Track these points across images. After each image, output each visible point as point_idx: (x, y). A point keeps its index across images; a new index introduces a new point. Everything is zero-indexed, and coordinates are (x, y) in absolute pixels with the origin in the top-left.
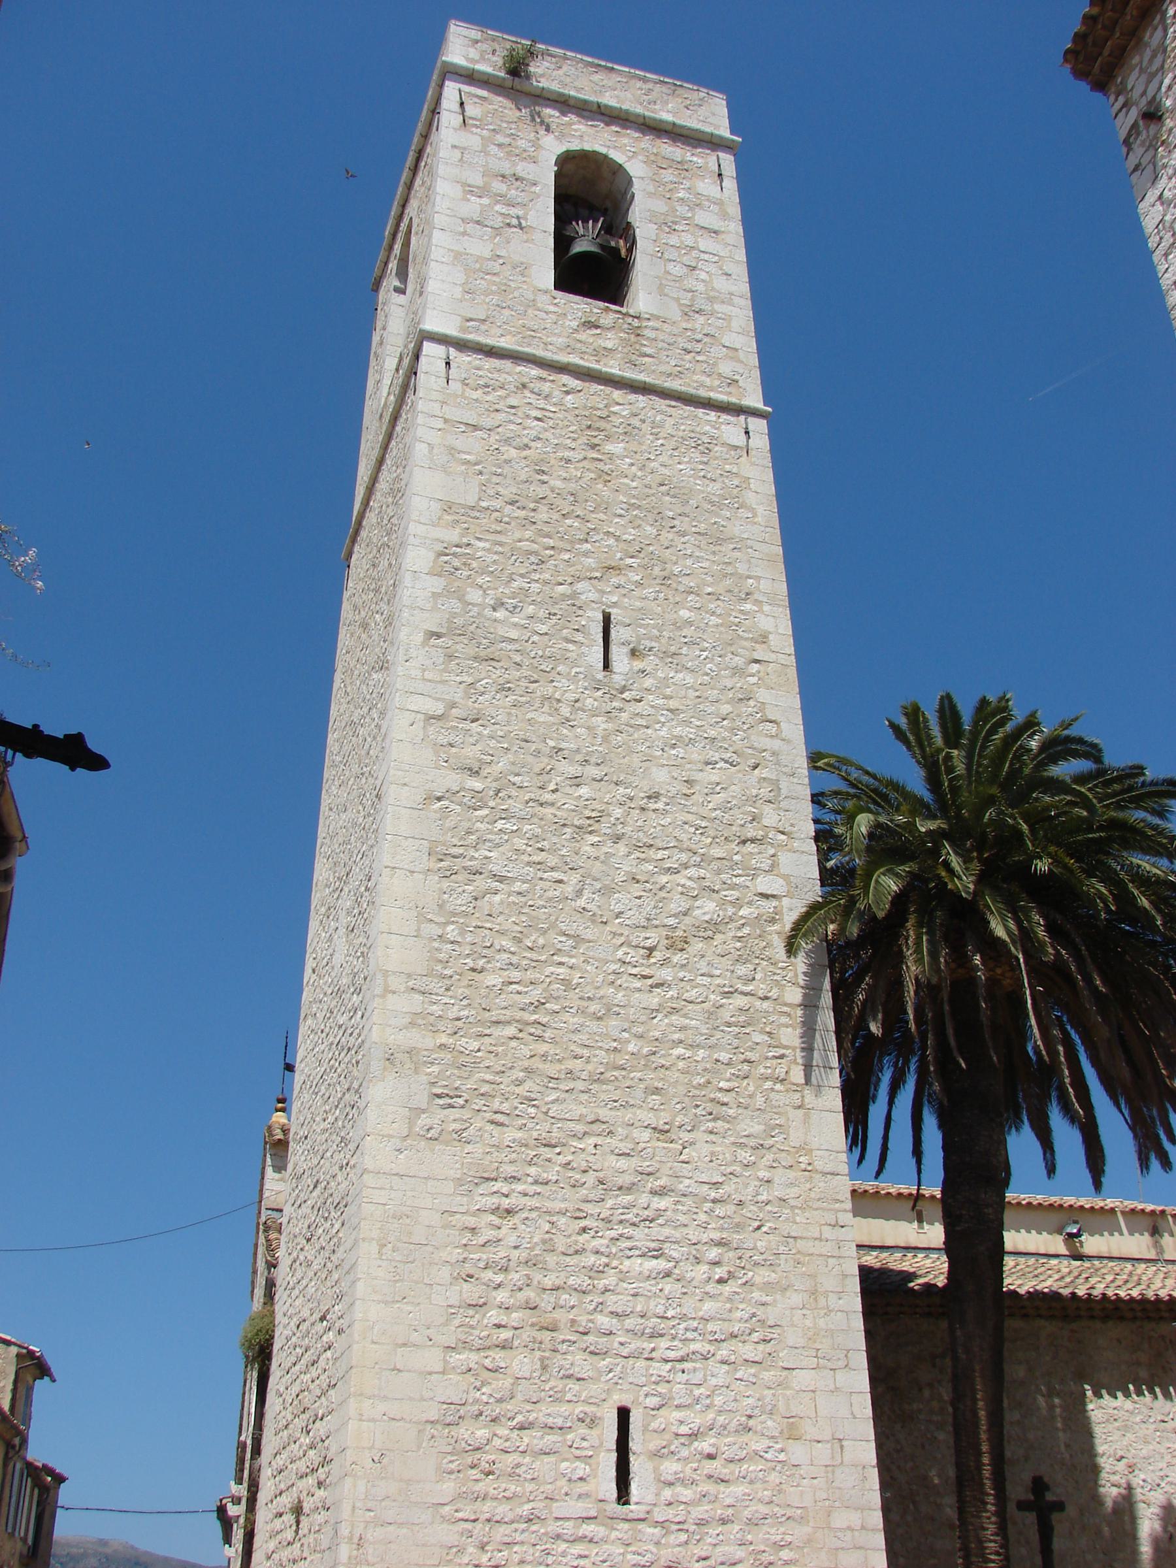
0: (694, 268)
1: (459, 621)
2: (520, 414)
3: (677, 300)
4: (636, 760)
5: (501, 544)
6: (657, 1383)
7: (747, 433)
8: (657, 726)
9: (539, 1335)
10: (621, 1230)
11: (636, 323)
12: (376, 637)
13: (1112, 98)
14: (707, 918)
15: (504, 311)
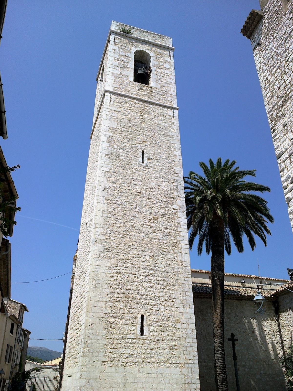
1: (112, 152)
2: (126, 108)
4: (148, 181)
5: (121, 136)
7: (174, 113)
8: (153, 174)
9: (125, 299)
12: (96, 155)
14: (162, 213)
15: (123, 86)
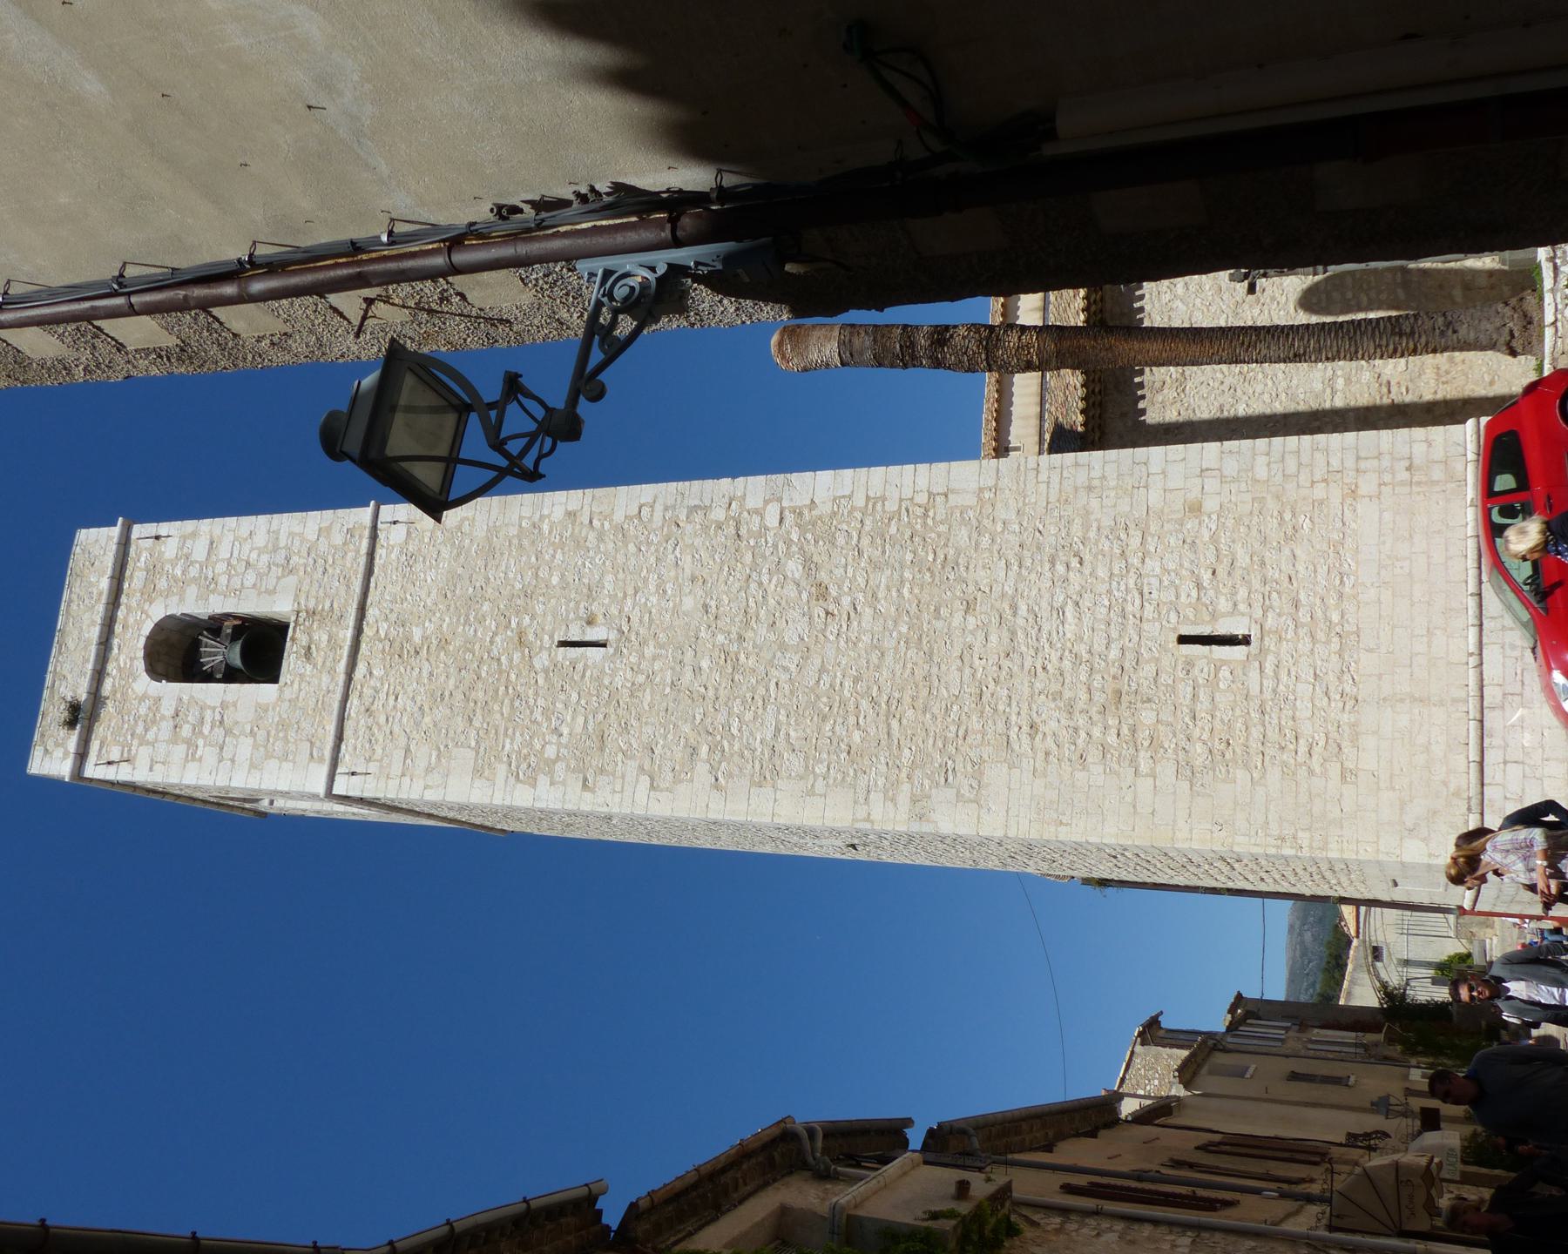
0: (248, 563)
3: (278, 578)
5: (506, 729)
9: (1125, 704)
11: (303, 615)
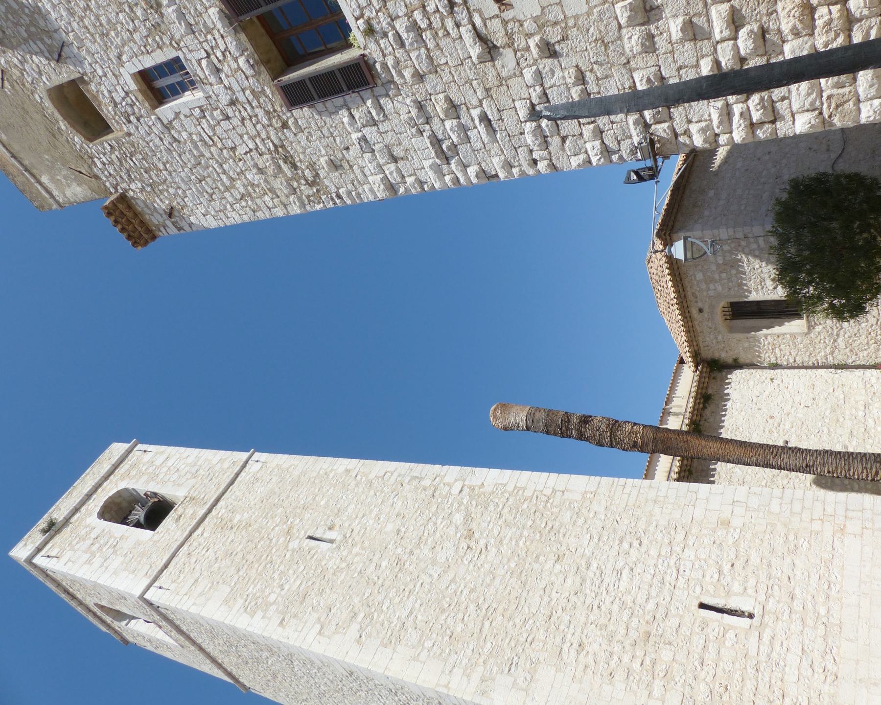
1: (281, 608)
6: (688, 586)
9: (651, 642)
10: (603, 589)
11: (188, 499)
13: (160, 234)
